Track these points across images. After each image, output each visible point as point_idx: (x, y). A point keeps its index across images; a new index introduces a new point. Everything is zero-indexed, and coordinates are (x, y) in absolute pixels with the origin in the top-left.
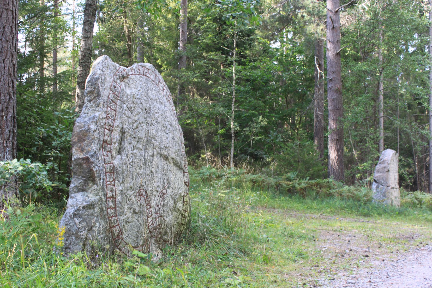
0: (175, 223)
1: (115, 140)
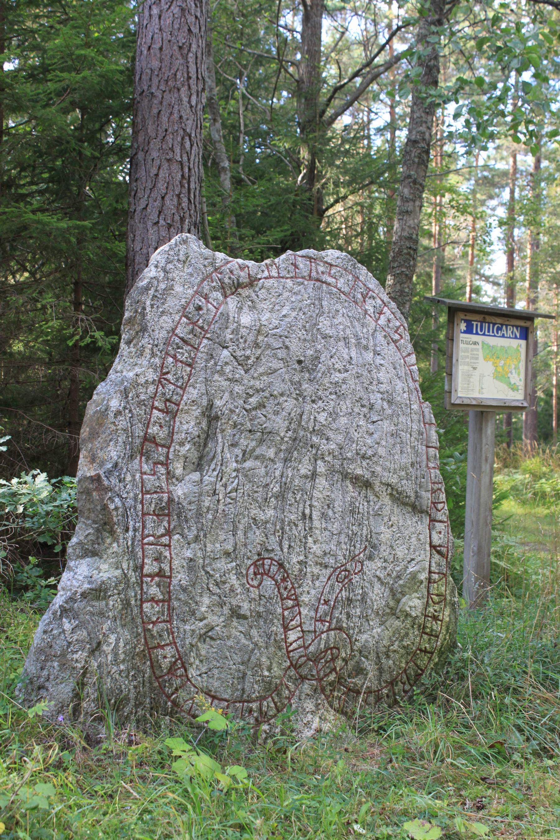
0: (395, 647)
1: (183, 436)
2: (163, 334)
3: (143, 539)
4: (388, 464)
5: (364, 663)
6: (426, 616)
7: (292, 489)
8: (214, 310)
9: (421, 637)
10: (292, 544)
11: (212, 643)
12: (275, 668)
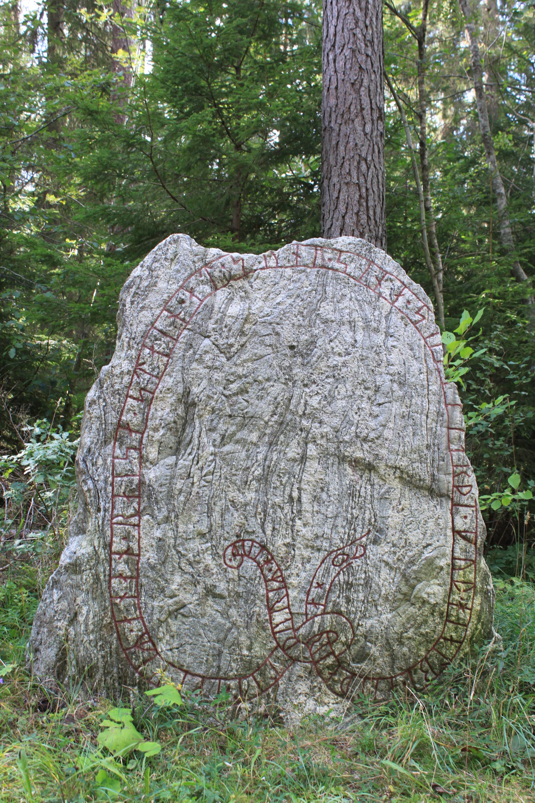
0: (410, 633)
1: (157, 422)
2: (142, 327)
3: (112, 519)
4: (396, 446)
5: (370, 648)
6: (449, 604)
7: (277, 473)
8: (198, 302)
9: (445, 624)
10: (277, 527)
11: (184, 620)
12: (257, 647)
